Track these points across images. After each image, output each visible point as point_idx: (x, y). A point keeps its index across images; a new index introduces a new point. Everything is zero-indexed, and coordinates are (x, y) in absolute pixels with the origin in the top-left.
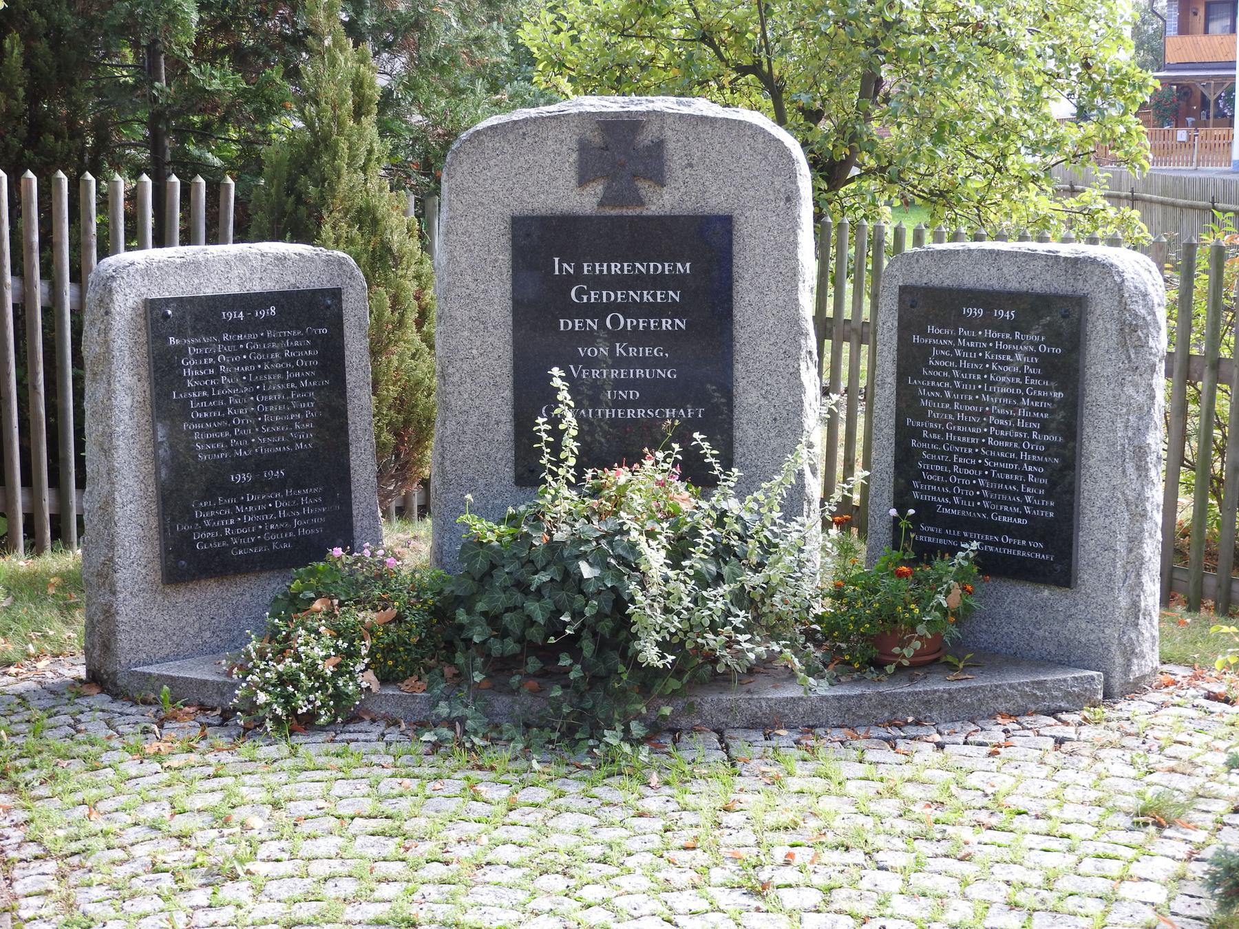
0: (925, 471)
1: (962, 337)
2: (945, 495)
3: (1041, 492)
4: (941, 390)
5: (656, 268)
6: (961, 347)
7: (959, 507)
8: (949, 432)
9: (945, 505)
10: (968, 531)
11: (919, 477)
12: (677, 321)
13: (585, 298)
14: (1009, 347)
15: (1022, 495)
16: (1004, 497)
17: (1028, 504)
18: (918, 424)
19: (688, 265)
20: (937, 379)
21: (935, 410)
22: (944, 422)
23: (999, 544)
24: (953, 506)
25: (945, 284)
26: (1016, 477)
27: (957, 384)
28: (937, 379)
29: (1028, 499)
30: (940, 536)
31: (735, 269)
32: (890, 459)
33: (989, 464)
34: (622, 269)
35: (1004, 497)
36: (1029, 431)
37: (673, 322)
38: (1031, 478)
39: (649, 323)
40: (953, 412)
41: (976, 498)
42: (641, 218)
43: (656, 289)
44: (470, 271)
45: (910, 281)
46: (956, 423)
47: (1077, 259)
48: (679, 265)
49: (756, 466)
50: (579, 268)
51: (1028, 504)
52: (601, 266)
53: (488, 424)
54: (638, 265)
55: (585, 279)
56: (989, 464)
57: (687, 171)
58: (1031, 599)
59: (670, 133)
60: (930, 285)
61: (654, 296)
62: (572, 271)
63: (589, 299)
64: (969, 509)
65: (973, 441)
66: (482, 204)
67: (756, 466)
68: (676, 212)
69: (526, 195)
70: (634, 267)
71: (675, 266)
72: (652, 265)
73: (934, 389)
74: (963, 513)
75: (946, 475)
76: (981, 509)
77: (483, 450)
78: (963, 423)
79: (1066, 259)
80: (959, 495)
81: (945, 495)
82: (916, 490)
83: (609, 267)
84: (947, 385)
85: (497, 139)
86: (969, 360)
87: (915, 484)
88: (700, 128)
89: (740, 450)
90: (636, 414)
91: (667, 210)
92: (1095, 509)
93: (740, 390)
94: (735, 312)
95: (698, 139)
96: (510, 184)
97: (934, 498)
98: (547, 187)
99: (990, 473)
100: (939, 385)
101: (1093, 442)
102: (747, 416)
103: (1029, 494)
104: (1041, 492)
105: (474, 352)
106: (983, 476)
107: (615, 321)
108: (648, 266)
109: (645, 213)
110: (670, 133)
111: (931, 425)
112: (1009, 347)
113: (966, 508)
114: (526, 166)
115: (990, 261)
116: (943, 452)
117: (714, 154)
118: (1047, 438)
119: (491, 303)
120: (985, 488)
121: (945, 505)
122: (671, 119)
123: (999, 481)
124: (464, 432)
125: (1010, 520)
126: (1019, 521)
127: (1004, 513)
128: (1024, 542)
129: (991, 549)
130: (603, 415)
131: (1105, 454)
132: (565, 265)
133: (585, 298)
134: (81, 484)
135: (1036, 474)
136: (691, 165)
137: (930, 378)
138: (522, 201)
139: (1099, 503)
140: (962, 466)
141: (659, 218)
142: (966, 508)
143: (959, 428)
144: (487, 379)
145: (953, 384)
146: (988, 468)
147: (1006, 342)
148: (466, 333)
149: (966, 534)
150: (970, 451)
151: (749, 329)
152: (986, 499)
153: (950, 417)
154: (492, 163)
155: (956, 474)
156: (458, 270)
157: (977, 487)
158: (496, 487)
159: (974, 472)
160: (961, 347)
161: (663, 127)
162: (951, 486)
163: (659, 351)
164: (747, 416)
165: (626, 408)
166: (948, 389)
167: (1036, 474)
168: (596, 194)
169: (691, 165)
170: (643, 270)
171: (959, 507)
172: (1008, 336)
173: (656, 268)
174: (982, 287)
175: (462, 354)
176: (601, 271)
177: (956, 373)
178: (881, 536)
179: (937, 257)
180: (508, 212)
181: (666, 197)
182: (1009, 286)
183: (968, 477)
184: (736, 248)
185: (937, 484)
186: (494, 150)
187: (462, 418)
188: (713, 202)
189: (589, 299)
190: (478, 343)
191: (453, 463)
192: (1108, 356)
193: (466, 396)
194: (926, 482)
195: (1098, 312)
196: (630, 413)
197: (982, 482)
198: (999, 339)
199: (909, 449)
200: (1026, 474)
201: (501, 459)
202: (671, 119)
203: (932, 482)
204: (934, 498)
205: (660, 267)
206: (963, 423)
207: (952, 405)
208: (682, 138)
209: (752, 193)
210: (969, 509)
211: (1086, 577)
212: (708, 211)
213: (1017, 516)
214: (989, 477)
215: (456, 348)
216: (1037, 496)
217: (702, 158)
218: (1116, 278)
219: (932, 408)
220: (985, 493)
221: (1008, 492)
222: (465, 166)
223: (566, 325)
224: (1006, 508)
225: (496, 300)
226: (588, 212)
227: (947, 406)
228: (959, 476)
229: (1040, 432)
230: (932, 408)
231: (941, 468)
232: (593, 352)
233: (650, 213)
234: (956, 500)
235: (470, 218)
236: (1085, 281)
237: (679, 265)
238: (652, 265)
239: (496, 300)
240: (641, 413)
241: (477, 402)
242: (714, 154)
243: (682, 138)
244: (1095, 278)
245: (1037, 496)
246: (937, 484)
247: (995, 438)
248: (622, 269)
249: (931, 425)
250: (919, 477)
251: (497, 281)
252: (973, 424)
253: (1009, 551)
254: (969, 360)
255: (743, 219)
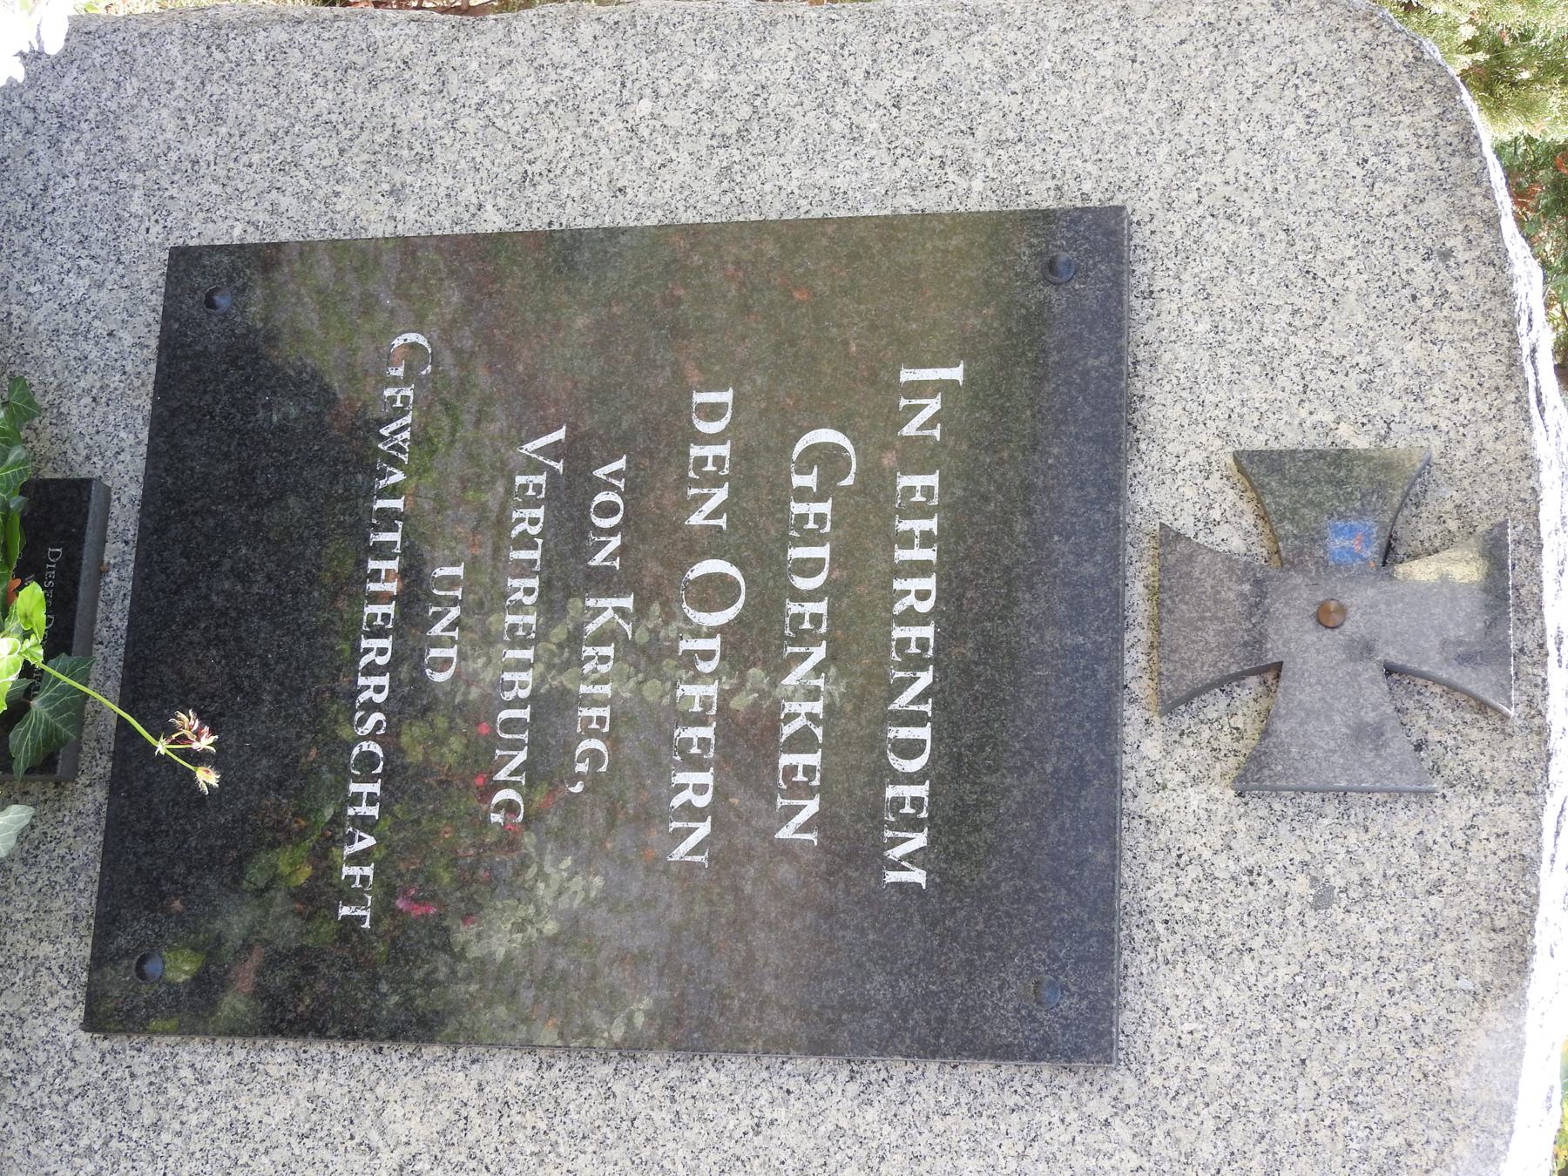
5: (910, 749)
12: (703, 829)
13: (809, 481)
19: (918, 876)
31: (901, 1069)
34: (910, 618)
37: (697, 814)
39: (701, 721)
42: (1114, 688)
43: (828, 750)
44: (930, 78)
48: (919, 840)
49: (156, 1127)
50: (918, 456)
52: (927, 539)
53: (395, 161)
54: (925, 678)
55: (876, 484)
57: (1301, 885)
59: (1457, 816)
61: (802, 741)
62: (910, 430)
63: (803, 495)
66: (1178, 109)
67: (156, 1127)
68: (1133, 838)
69: (1209, 265)
70: (918, 664)
71: (914, 824)
72: (924, 733)
77: (308, 148)
83: (921, 569)
85: (1426, 156)
88: (1478, 940)
89: (221, 1066)
90: (372, 670)
91: (1141, 801)
93: (436, 1074)
94: (732, 1064)
95: (1434, 930)
96: (1248, 206)
98: (1237, 342)
102: (339, 1098)
105: (645, 106)
107: (714, 592)
108: (916, 720)
109: (1133, 715)
110: (1457, 816)
114: (1320, 267)
117: (1370, 996)
119: (812, 154)
122: (1515, 824)
124: (373, 84)
130: (383, 552)
132: (933, 405)
133: (809, 481)
134: (1542, 411)
136: (1323, 899)
138: (1185, 256)
141: (1111, 771)
144: (547, 151)
148: (709, 76)
151: (662, 1117)
154: (1333, 142)
156: (935, 38)
158: (186, 195)
161: (1479, 787)
163: (595, 756)
164: (339, 1098)
165: (399, 633)
168: (1210, 525)
169: (1323, 899)
170: (902, 701)
173: (910, 749)
175: (639, 65)
176: (907, 541)
180: (1140, 206)
181: (1196, 798)
184: (982, 1074)
186: (1384, 149)
187: (421, 76)
188: (1171, 986)
189: (803, 495)
190: (673, 120)
191: (275, 54)
193: (495, 84)
196: (377, 650)
201: (274, 210)
202: (1515, 824)
205: (915, 765)
208: (1437, 868)
209: (1205, 1151)
212: (1137, 963)
215: (661, 45)
217: (1350, 947)
222: (1320, 50)
223: (713, 412)
225: (822, 174)
226: (1140, 499)
232: (608, 510)
233: (1131, 733)
235: (1125, 73)
237: (919, 840)
238: (924, 733)
239: (822, 174)
240: (375, 689)
241: (470, 123)
242: (1370, 996)
243: (1437, 868)
248: (910, 618)
251: (889, 175)
255: (1100, 1107)
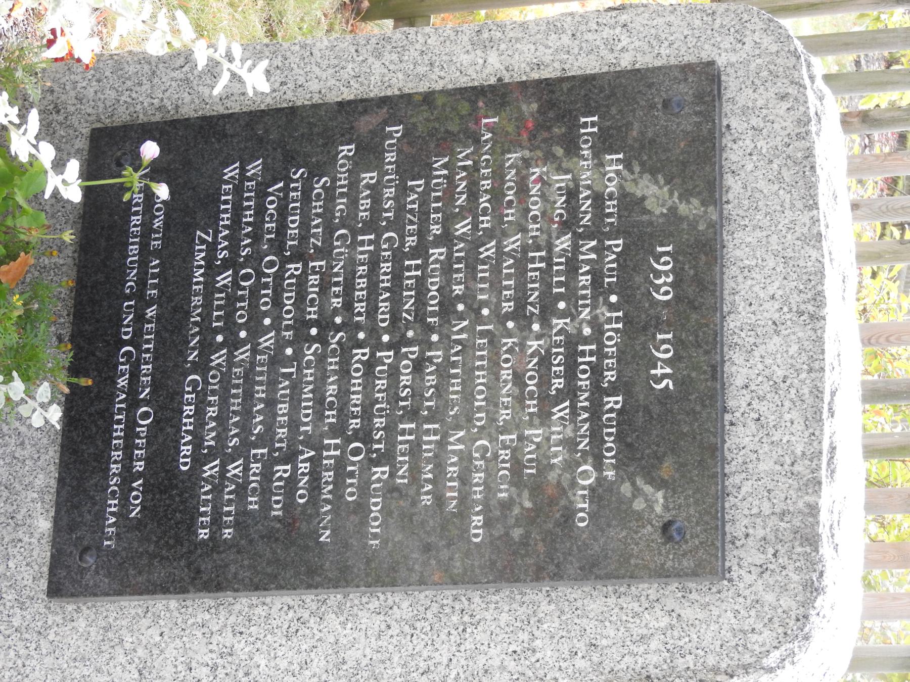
0: (286, 189)
1: (600, 250)
2: (234, 247)
3: (253, 503)
4: (472, 208)
6: (576, 248)
7: (210, 289)
8: (376, 242)
9: (212, 248)
10: (159, 318)
11: (272, 175)
14: (584, 381)
15: (242, 451)
16: (236, 404)
17: (223, 471)
18: (390, 157)
20: (497, 195)
21: (424, 199)
22: (398, 224)
23: (133, 403)
24: (212, 270)
25: (729, 180)
26: (282, 432)
27: (488, 251)
28: (497, 195)
29: (234, 469)
30: (144, 246)
32: (314, 86)
33: (309, 355)
35: (236, 404)
36: (387, 457)
38: (282, 470)
40: (420, 251)
41: (230, 328)
45: (731, 84)
46: (398, 257)
47: (812, 540)
51: (223, 471)
56: (309, 355)
58: (28, 487)
60: (727, 140)
64: (206, 317)
65: (360, 307)
73: (473, 193)
74: (197, 300)
75: (278, 246)
76: (207, 348)
78: (397, 276)
79: (813, 510)
80: (236, 284)
81: (234, 247)
82: (243, 169)
84: (486, 222)
86: (546, 273)
87: (255, 168)
92: (228, 639)
97: (225, 219)
99: (288, 362)
100: (484, 201)
101: (378, 622)
103: (246, 469)
104: (253, 503)
106: (280, 344)
111: (389, 192)
112: (584, 381)
113: (208, 305)
115: (795, 299)
116: (329, 230)
118: (376, 504)
120: (255, 351)
121: (212, 248)
123: (272, 384)
125: (188, 424)
126: (186, 450)
127: (201, 405)
128: (139, 466)
129: (122, 382)
131: (352, 655)
135: (291, 483)
137: (499, 175)
139: (241, 648)
140: (302, 282)
142: (208, 305)
143: (386, 267)
145: (490, 234)
146: (298, 356)
147: (597, 371)
149: (151, 312)
150: (337, 302)
152: (231, 356)
153: (411, 241)
155: (282, 269)
157: (257, 332)
159: (288, 319)
160: (576, 248)
162: (255, 259)
166: (475, 226)
167: (291, 483)
171: (210, 289)
172: (610, 376)
174: (729, 284)
177: (513, 243)
178: (147, 86)
179: (797, 149)
182: (737, 356)
183: (277, 302)
185: (258, 224)
192: (581, 646)
194: (262, 194)
195: (688, 613)
197: (267, 341)
198: (600, 354)
199: (330, 143)
200: (291, 457)
203: (260, 211)
204: (225, 219)
206: (397, 276)
207: (437, 243)
210: (206, 317)
211: (81, 624)
213: (197, 442)
214: (276, 360)
216: (242, 490)
218: (775, 655)
219: (428, 189)
220: (243, 354)
221: (247, 413)
224: (212, 411)
227: (436, 229)
228: (279, 277)
229: (391, 490)
230: (428, 189)
231: (293, 230)
234: (224, 279)
236: (763, 570)
244: (769, 598)
245: (242, 490)
246: (258, 224)
247: (370, 365)
249: (389, 192)
250: (272, 175)
252: (396, 301)
253: (119, 430)
254: (546, 273)
